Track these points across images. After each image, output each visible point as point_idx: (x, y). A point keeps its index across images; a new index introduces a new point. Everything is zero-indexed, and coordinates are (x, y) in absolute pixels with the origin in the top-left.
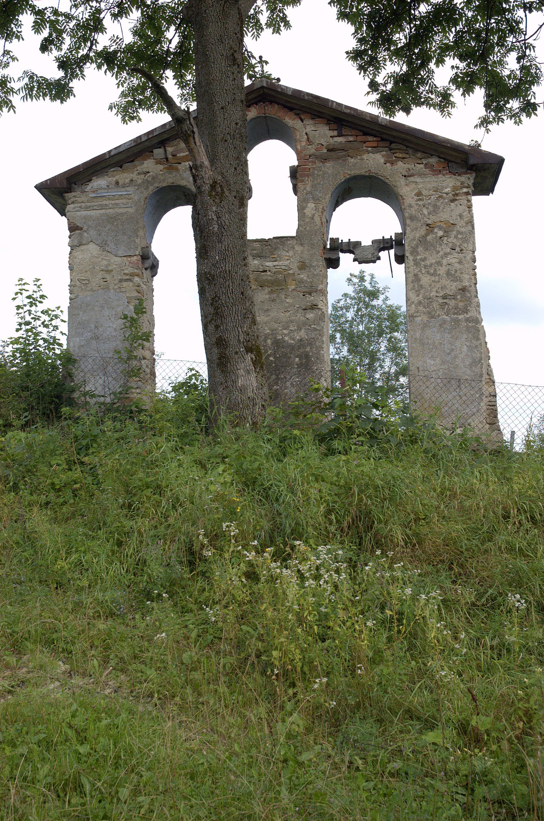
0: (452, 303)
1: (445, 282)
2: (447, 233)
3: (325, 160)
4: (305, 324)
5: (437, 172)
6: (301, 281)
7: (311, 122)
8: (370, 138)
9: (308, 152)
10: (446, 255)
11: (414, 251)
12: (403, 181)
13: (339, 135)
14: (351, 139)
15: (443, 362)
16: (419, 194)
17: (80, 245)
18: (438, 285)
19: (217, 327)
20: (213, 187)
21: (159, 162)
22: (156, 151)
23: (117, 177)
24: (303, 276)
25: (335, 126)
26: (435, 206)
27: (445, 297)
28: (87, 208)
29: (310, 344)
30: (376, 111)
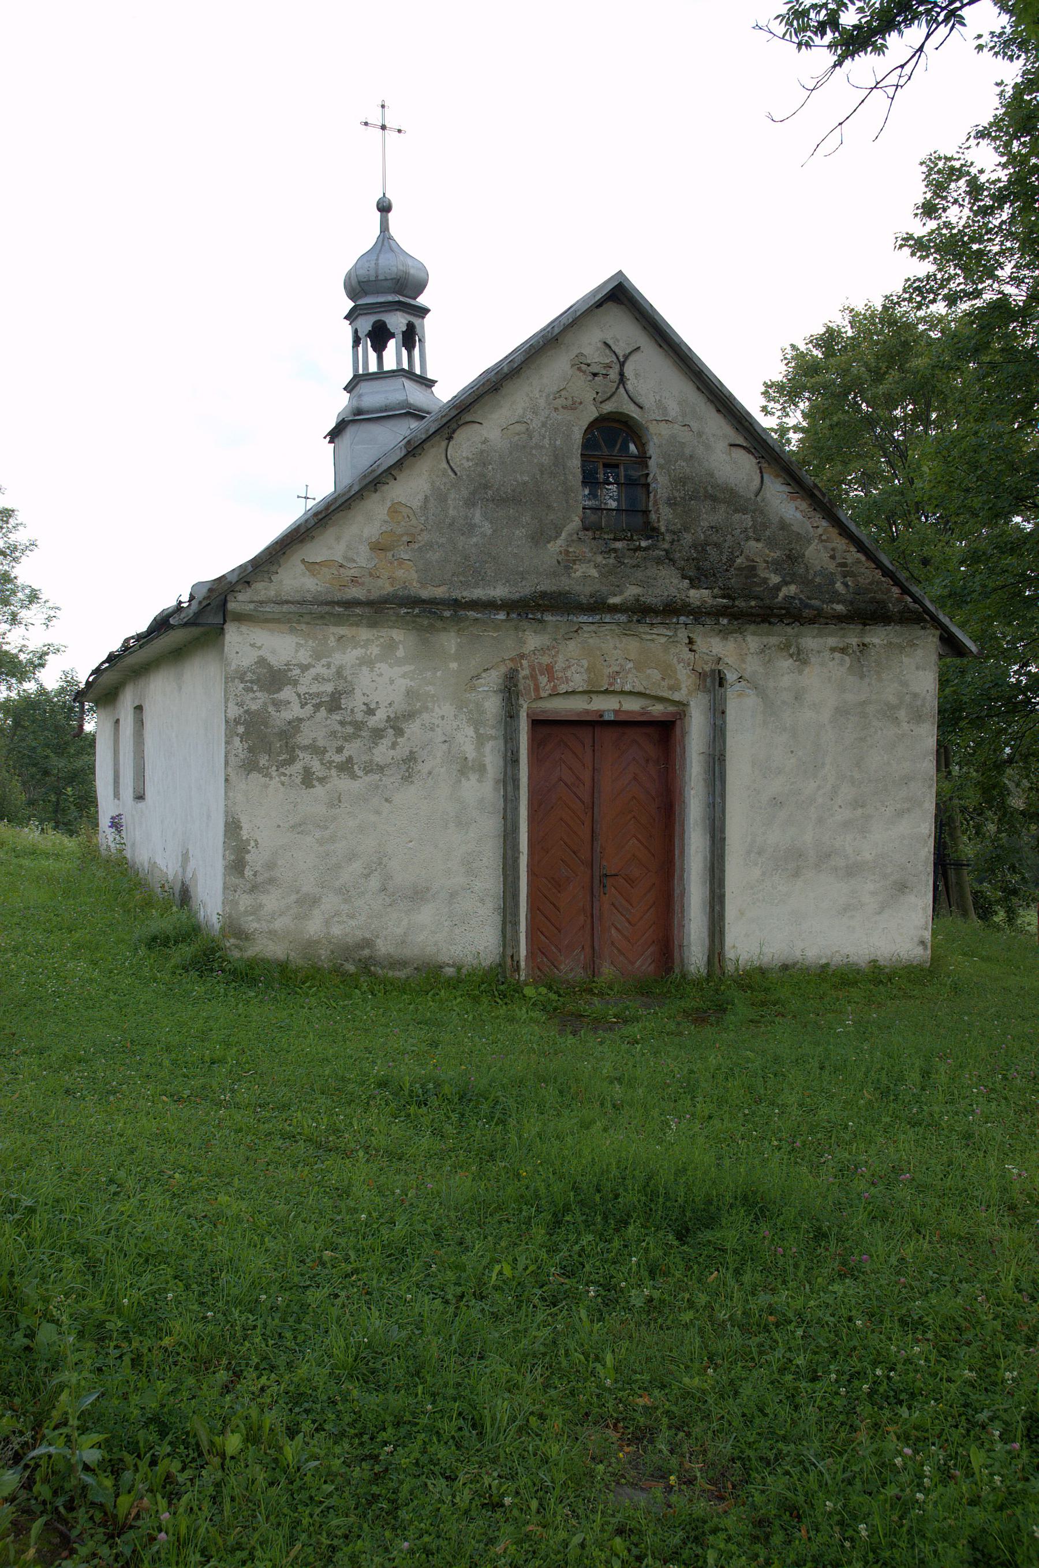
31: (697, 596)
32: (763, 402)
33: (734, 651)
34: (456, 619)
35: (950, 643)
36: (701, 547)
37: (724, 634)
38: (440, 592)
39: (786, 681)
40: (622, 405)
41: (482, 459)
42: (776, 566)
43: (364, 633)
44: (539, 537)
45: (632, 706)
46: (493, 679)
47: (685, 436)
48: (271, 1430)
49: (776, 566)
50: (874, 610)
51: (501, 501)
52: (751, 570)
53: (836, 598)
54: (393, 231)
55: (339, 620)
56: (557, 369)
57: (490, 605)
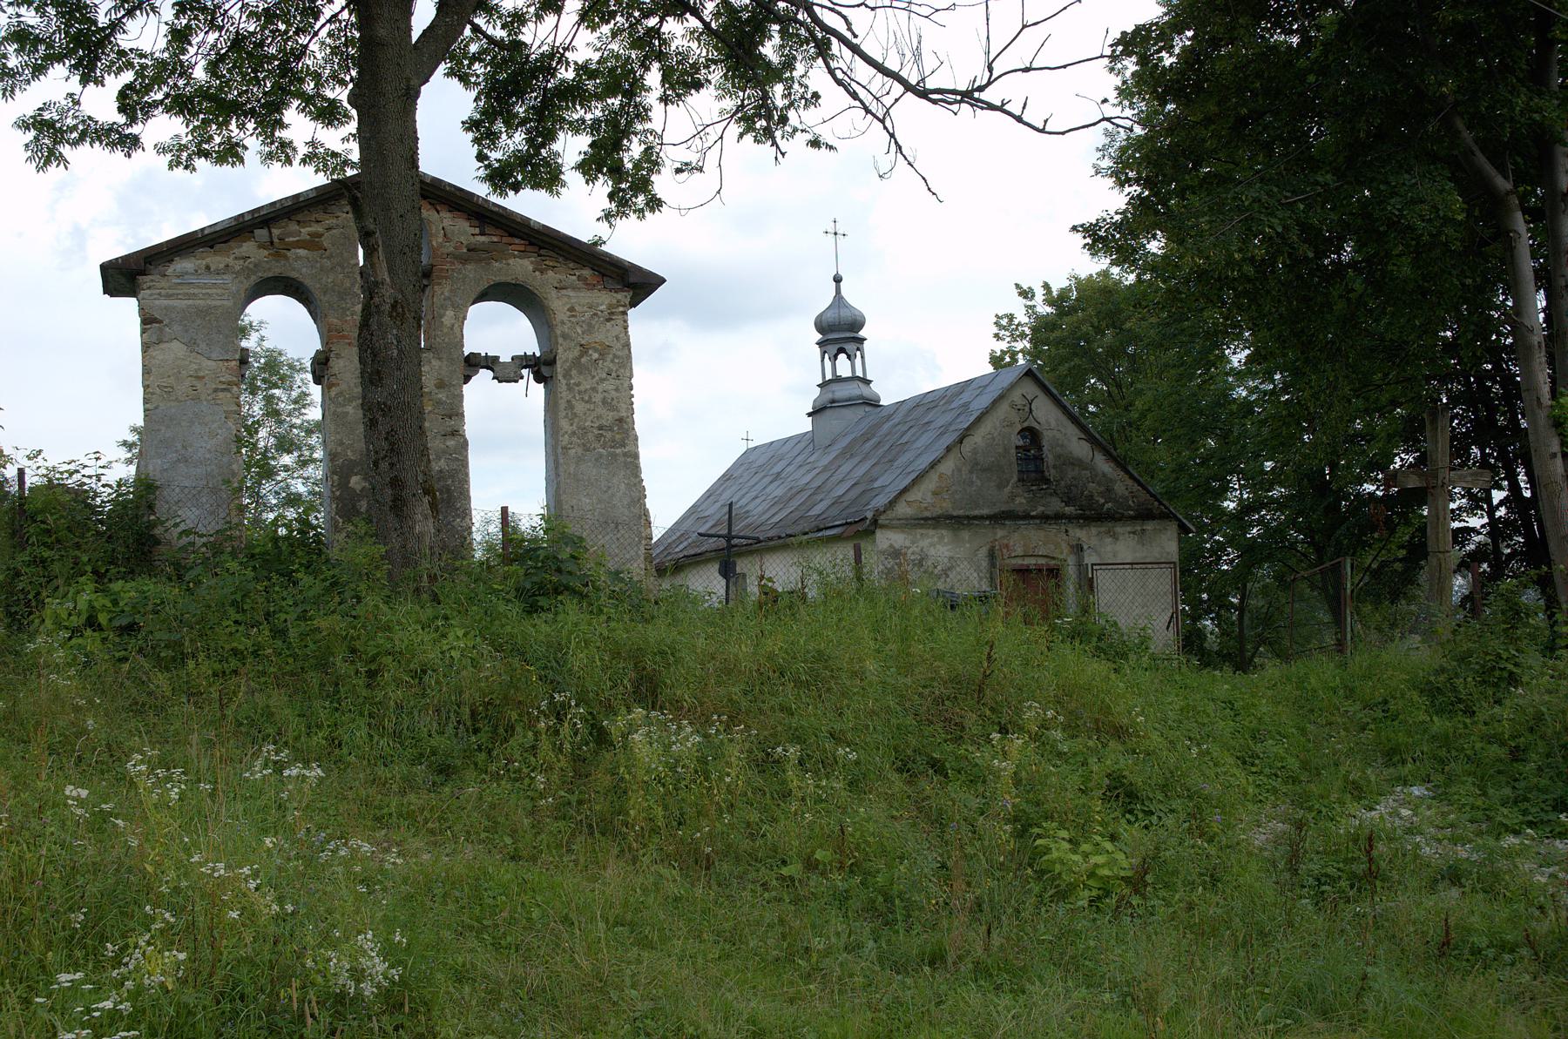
0: (609, 435)
1: (601, 410)
2: (602, 355)
3: (464, 260)
4: (444, 452)
5: (591, 287)
6: (439, 402)
7: (448, 215)
8: (517, 241)
9: (446, 251)
10: (602, 380)
11: (567, 375)
12: (554, 293)
13: (482, 234)
14: (495, 239)
15: (600, 501)
16: (572, 309)
17: (160, 342)
18: (594, 414)
19: (392, 465)
20: (394, 307)
21: (261, 246)
22: (258, 232)
23: (208, 260)
24: (442, 396)
25: (476, 223)
26: (590, 325)
27: (600, 428)
28: (168, 296)
29: (452, 477)
30: (482, 190)
31: (1068, 510)
32: (995, 330)
34: (969, 525)
35: (1184, 529)
36: (1069, 487)
37: (1081, 527)
38: (961, 512)
39: (1109, 548)
40: (1031, 423)
41: (975, 451)
42: (1102, 494)
43: (931, 532)
44: (1000, 486)
45: (1042, 561)
46: (984, 552)
47: (1058, 435)
49: (1102, 494)
50: (1145, 515)
51: (984, 470)
52: (1091, 497)
53: (1130, 508)
54: (844, 293)
55: (922, 526)
56: (1004, 407)
57: (982, 518)
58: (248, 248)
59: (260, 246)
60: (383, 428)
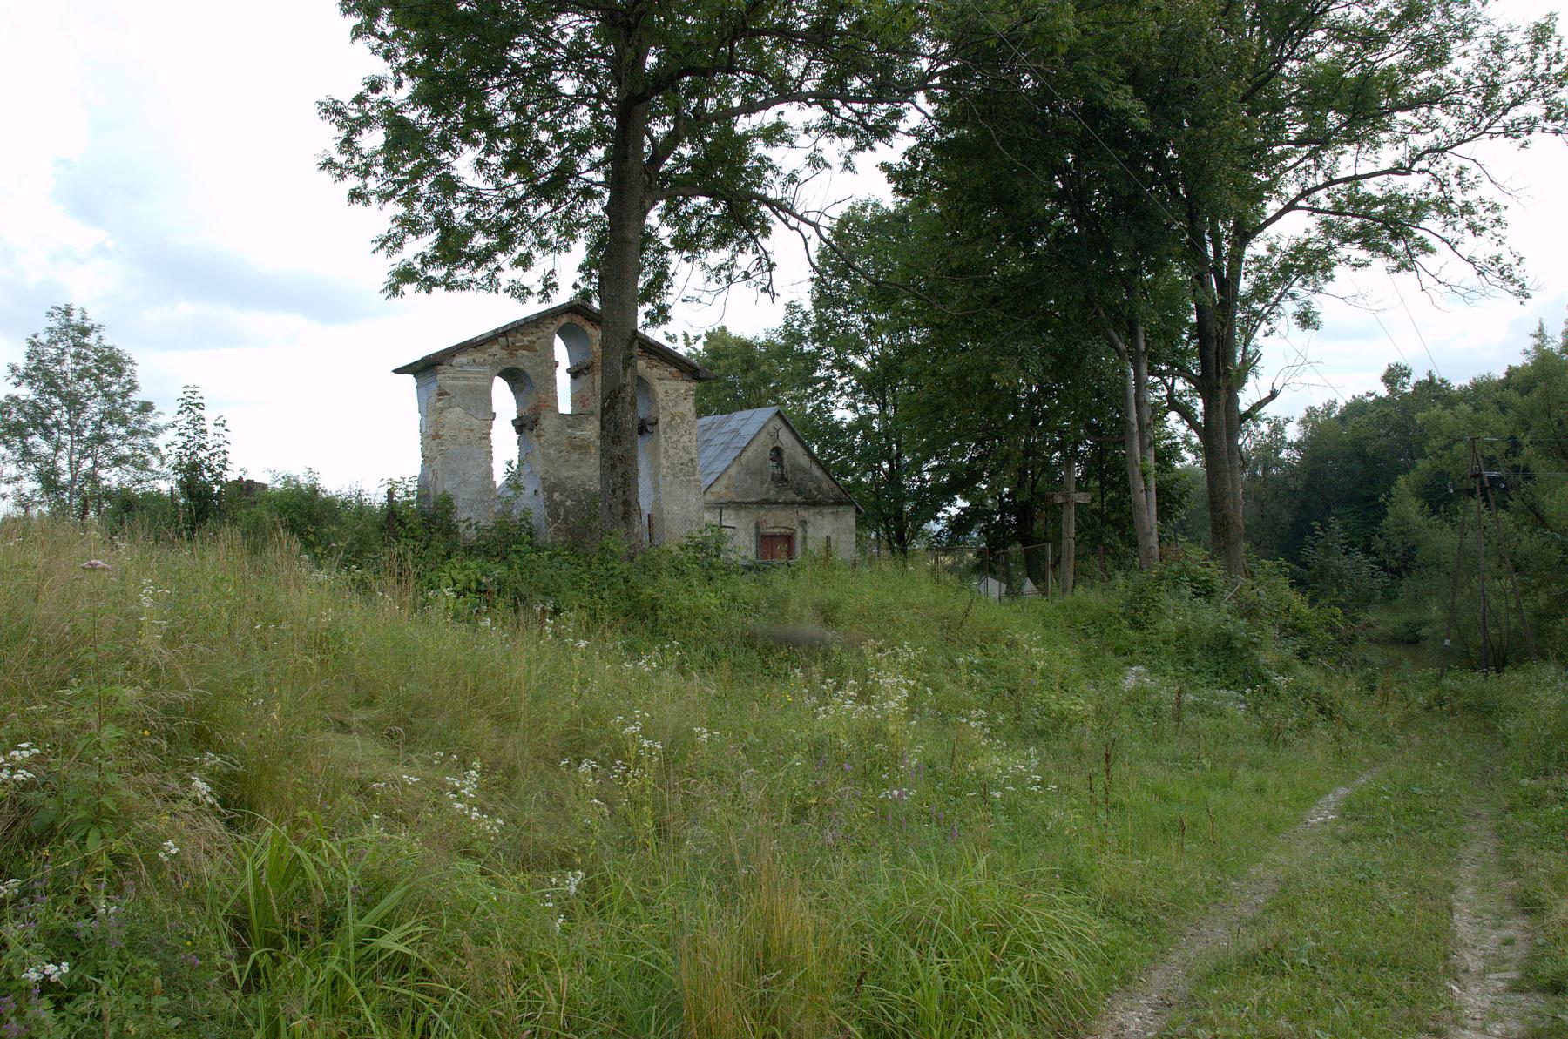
5: (676, 378)
31: (799, 499)
33: (807, 514)
35: (858, 511)
44: (762, 483)
46: (752, 525)
48: (122, 523)
56: (764, 433)
58: (496, 349)
59: (514, 352)
60: (620, 470)
